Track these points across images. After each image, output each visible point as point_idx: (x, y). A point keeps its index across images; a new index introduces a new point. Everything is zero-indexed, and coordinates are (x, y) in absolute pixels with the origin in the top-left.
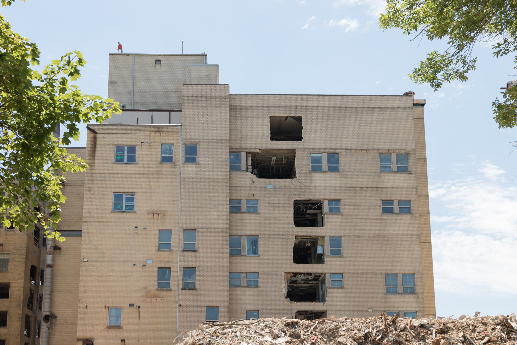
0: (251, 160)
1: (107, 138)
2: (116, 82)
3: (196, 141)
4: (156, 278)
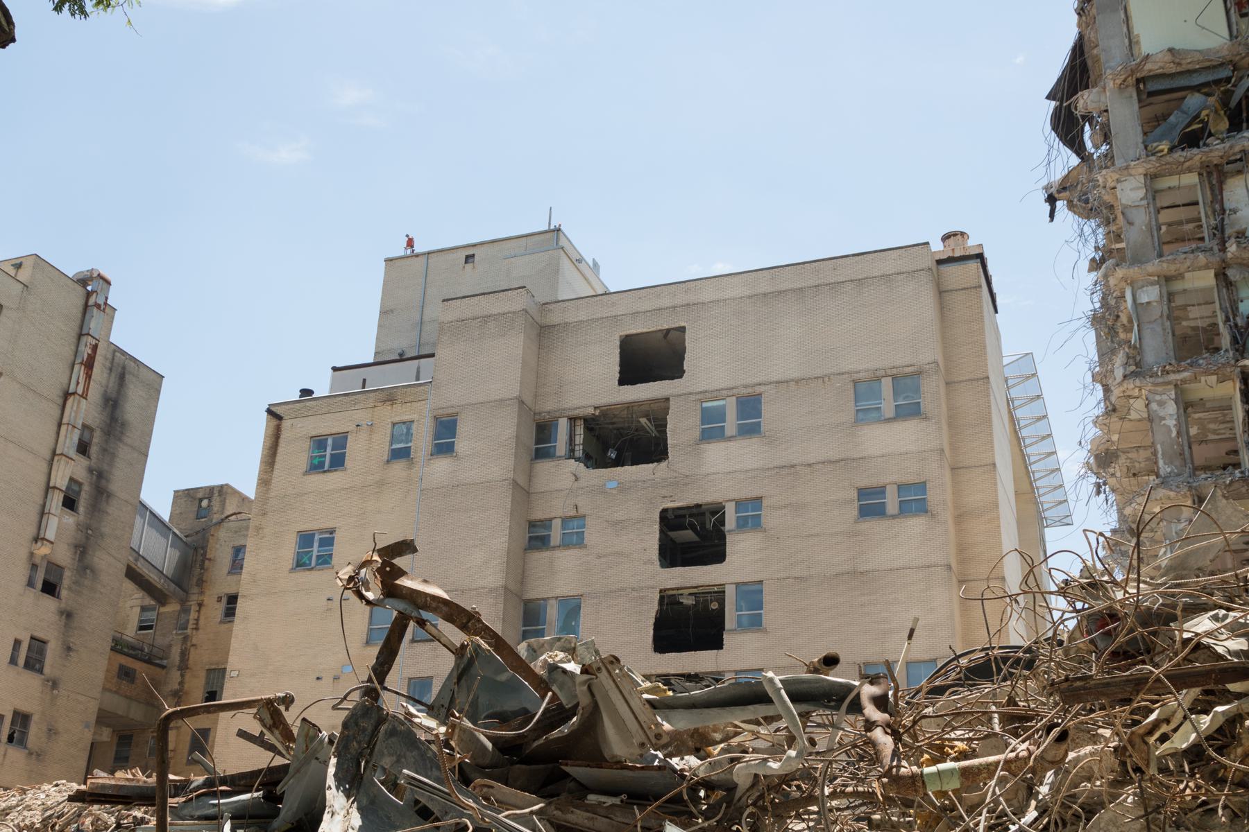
2: (392, 311)
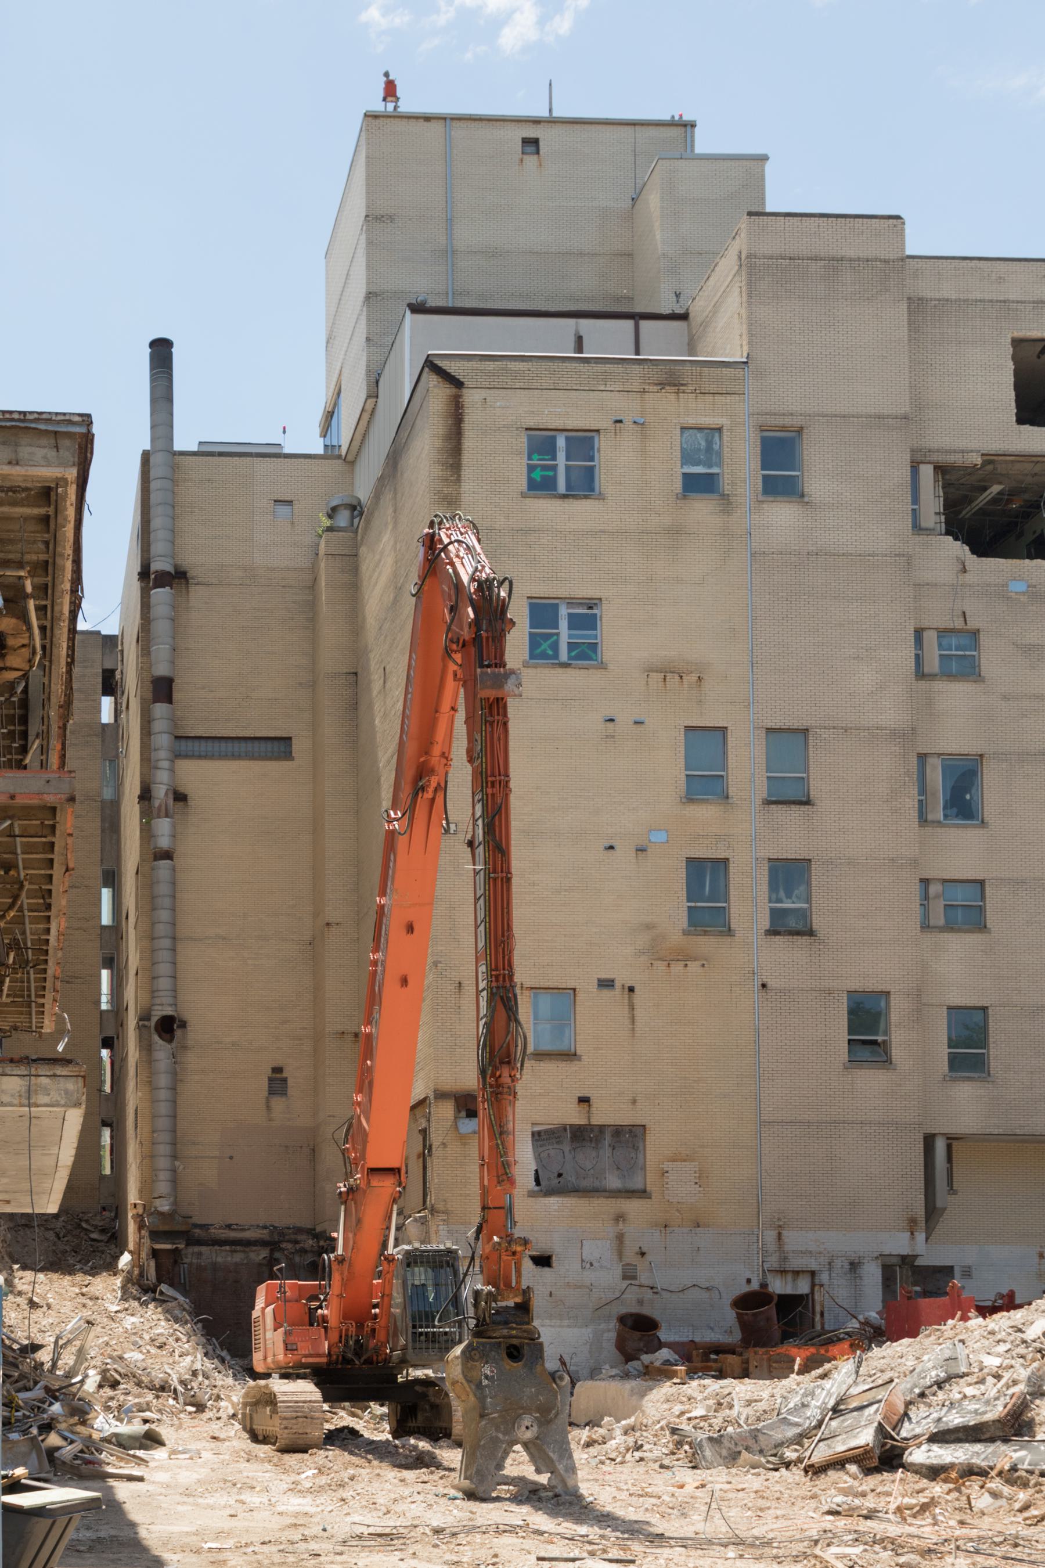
0: (941, 494)
1: (498, 404)
2: (391, 218)
3: (797, 421)
4: (683, 894)
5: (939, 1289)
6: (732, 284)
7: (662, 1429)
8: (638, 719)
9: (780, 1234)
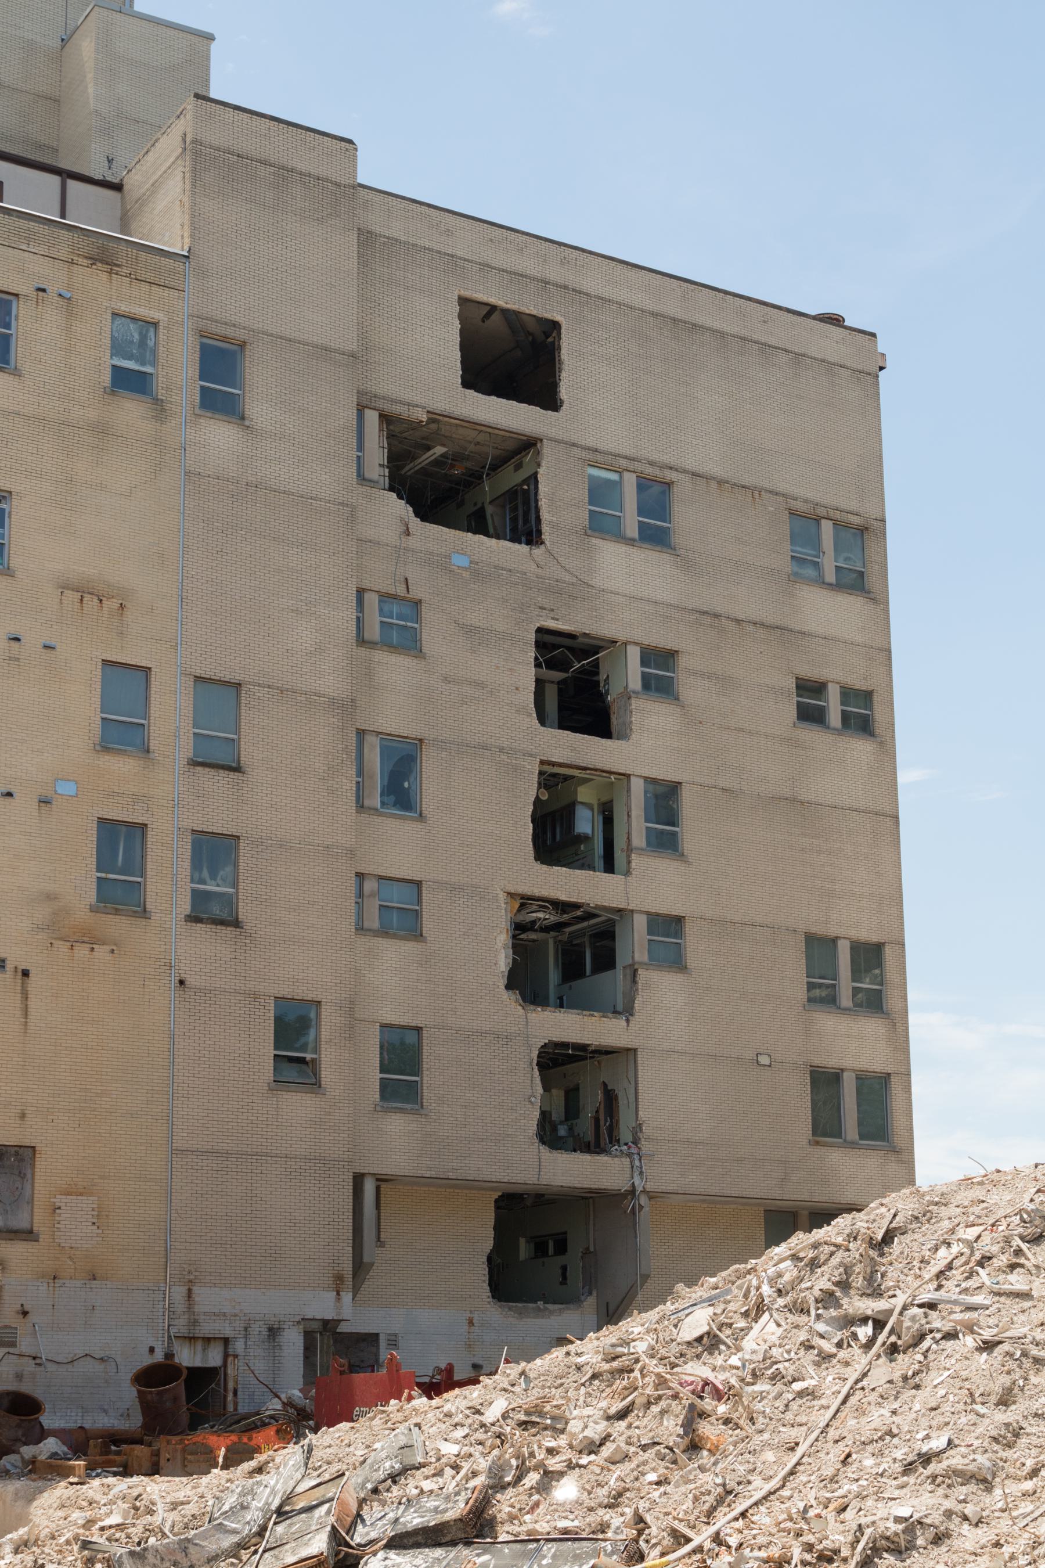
0: (386, 445)
3: (240, 335)
5: (362, 1361)
6: (174, 167)
7: (68, 1542)
8: (48, 643)
9: (190, 1290)
